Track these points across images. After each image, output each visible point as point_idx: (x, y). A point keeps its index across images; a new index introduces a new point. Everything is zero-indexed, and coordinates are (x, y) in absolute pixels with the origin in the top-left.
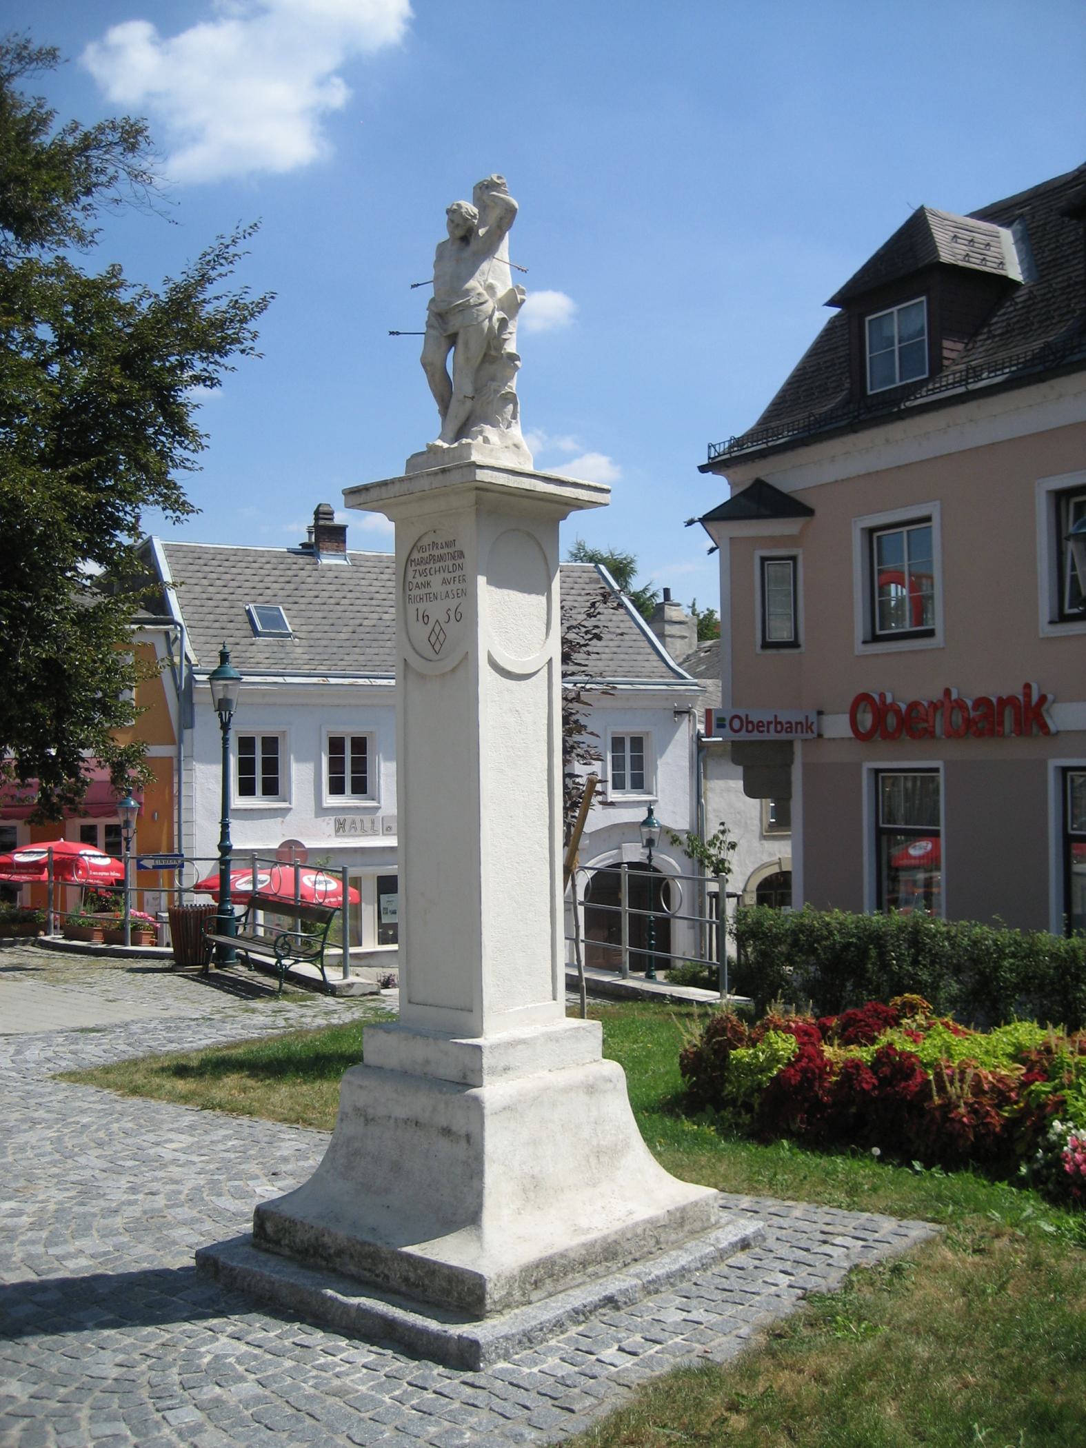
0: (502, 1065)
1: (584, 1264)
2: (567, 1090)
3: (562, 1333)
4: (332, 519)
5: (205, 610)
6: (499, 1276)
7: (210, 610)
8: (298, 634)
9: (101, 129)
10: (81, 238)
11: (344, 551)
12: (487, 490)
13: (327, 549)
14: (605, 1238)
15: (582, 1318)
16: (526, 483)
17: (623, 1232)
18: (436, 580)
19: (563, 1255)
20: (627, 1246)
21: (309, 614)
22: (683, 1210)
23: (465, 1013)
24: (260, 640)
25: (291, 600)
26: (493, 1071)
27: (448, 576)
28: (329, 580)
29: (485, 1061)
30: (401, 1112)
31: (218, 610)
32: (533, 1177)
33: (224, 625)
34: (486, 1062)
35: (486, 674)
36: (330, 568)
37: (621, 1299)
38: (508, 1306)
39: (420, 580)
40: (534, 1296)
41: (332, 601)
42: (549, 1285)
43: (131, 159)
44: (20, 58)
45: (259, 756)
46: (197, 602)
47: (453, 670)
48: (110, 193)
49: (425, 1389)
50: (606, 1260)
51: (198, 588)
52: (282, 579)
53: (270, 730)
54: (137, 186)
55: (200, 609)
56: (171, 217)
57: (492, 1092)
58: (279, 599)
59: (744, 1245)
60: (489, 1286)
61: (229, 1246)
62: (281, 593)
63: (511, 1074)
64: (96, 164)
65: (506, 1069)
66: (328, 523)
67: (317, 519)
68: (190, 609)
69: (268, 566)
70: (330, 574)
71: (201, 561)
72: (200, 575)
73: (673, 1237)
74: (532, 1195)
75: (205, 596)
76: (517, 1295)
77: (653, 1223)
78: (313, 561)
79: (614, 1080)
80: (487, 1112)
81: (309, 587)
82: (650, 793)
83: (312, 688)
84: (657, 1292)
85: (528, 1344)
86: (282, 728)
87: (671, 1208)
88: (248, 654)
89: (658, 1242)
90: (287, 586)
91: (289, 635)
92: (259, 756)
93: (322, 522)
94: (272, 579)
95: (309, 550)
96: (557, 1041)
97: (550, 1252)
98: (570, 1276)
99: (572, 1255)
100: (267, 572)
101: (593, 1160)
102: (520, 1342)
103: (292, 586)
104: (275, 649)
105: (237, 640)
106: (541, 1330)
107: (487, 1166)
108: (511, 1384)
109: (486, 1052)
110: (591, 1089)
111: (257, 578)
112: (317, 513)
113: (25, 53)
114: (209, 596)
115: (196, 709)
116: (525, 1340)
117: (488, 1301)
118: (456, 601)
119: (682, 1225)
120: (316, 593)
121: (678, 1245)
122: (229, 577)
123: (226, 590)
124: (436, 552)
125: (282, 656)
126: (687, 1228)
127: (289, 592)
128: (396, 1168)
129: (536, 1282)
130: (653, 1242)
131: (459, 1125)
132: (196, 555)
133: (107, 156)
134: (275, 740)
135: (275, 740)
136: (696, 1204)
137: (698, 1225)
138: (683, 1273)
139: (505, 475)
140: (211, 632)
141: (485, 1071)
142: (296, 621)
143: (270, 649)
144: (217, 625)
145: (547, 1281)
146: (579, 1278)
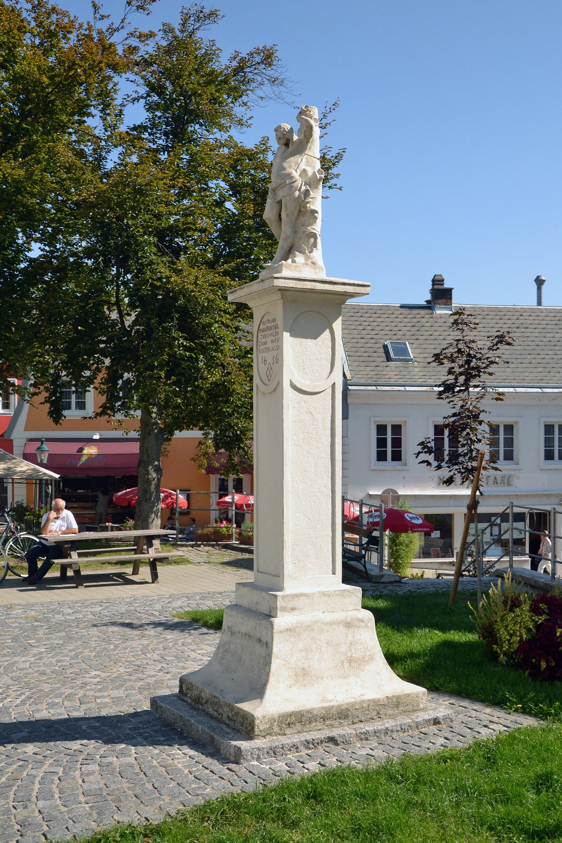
0: (290, 606)
1: (324, 719)
2: (330, 624)
3: (297, 752)
4: (443, 284)
5: (359, 345)
6: (264, 717)
7: (362, 345)
8: (417, 360)
9: (251, 54)
10: (240, 123)
11: (451, 304)
12: (286, 290)
13: (440, 304)
14: (339, 706)
15: (311, 746)
16: (309, 285)
17: (353, 704)
18: (269, 340)
19: (309, 712)
20: (355, 713)
21: (425, 346)
22: (398, 697)
23: (276, 578)
24: (391, 364)
25: (414, 337)
26: (284, 609)
27: (274, 338)
28: (440, 324)
29: (278, 603)
30: (244, 630)
31: (368, 345)
32: (303, 669)
33: (370, 354)
34: (279, 604)
35: (288, 393)
36: (441, 316)
37: (340, 740)
38: (270, 734)
39: (263, 340)
40: (288, 731)
41: (441, 338)
42: (298, 726)
43: (270, 72)
44: (198, 19)
45: (389, 437)
46: (355, 341)
47: (275, 390)
48: (259, 92)
49: (207, 769)
50: (340, 718)
51: (356, 332)
52: (410, 324)
53: (396, 421)
54: (275, 88)
55: (356, 345)
56: (294, 105)
57: (281, 621)
58: (406, 337)
59: (436, 722)
60: (257, 722)
61: (164, 698)
62: (408, 333)
63: (296, 612)
64: (250, 76)
65: (293, 609)
66: (440, 287)
67: (433, 285)
68: (350, 345)
69: (402, 316)
70: (440, 320)
71: (359, 315)
72: (357, 323)
73: (390, 712)
74: (301, 679)
75: (360, 336)
76: (276, 729)
77: (375, 702)
78: (430, 311)
79: (366, 621)
80: (275, 630)
81: (427, 329)
82: (518, 464)
83: (416, 393)
84: (367, 739)
85: (273, 755)
86: (404, 419)
87: (390, 695)
88: (384, 373)
89: (378, 713)
90: (413, 329)
91: (411, 360)
92: (389, 437)
93: (436, 287)
94: (403, 324)
95: (429, 306)
96: (329, 596)
97: (301, 709)
98: (314, 724)
99: (315, 712)
100: (400, 320)
101: (346, 664)
102: (268, 753)
103: (416, 329)
104: (402, 369)
105: (378, 364)
106: (282, 748)
107: (273, 660)
108: (250, 772)
109: (279, 599)
110: (348, 625)
111: (393, 324)
112: (433, 281)
113: (201, 15)
114: (362, 336)
115: (350, 406)
116: (271, 752)
117: (256, 730)
118: (276, 352)
119: (397, 706)
120: (431, 333)
121: (392, 716)
122: (375, 324)
123: (373, 332)
124: (269, 325)
125: (406, 373)
126: (401, 708)
127: (413, 333)
128: (240, 660)
129: (289, 724)
130: (375, 713)
131: (264, 639)
132: (356, 311)
133: (256, 71)
134: (400, 426)
135: (400, 426)
136: (409, 695)
137: (410, 708)
138: (386, 731)
139: (294, 281)
140: (362, 359)
141: (279, 609)
142: (417, 351)
143: (398, 369)
144: (366, 354)
145: (297, 724)
146: (319, 725)
